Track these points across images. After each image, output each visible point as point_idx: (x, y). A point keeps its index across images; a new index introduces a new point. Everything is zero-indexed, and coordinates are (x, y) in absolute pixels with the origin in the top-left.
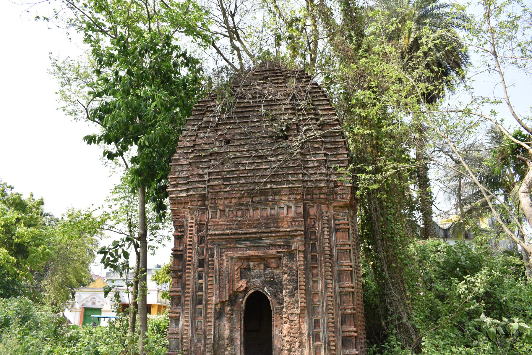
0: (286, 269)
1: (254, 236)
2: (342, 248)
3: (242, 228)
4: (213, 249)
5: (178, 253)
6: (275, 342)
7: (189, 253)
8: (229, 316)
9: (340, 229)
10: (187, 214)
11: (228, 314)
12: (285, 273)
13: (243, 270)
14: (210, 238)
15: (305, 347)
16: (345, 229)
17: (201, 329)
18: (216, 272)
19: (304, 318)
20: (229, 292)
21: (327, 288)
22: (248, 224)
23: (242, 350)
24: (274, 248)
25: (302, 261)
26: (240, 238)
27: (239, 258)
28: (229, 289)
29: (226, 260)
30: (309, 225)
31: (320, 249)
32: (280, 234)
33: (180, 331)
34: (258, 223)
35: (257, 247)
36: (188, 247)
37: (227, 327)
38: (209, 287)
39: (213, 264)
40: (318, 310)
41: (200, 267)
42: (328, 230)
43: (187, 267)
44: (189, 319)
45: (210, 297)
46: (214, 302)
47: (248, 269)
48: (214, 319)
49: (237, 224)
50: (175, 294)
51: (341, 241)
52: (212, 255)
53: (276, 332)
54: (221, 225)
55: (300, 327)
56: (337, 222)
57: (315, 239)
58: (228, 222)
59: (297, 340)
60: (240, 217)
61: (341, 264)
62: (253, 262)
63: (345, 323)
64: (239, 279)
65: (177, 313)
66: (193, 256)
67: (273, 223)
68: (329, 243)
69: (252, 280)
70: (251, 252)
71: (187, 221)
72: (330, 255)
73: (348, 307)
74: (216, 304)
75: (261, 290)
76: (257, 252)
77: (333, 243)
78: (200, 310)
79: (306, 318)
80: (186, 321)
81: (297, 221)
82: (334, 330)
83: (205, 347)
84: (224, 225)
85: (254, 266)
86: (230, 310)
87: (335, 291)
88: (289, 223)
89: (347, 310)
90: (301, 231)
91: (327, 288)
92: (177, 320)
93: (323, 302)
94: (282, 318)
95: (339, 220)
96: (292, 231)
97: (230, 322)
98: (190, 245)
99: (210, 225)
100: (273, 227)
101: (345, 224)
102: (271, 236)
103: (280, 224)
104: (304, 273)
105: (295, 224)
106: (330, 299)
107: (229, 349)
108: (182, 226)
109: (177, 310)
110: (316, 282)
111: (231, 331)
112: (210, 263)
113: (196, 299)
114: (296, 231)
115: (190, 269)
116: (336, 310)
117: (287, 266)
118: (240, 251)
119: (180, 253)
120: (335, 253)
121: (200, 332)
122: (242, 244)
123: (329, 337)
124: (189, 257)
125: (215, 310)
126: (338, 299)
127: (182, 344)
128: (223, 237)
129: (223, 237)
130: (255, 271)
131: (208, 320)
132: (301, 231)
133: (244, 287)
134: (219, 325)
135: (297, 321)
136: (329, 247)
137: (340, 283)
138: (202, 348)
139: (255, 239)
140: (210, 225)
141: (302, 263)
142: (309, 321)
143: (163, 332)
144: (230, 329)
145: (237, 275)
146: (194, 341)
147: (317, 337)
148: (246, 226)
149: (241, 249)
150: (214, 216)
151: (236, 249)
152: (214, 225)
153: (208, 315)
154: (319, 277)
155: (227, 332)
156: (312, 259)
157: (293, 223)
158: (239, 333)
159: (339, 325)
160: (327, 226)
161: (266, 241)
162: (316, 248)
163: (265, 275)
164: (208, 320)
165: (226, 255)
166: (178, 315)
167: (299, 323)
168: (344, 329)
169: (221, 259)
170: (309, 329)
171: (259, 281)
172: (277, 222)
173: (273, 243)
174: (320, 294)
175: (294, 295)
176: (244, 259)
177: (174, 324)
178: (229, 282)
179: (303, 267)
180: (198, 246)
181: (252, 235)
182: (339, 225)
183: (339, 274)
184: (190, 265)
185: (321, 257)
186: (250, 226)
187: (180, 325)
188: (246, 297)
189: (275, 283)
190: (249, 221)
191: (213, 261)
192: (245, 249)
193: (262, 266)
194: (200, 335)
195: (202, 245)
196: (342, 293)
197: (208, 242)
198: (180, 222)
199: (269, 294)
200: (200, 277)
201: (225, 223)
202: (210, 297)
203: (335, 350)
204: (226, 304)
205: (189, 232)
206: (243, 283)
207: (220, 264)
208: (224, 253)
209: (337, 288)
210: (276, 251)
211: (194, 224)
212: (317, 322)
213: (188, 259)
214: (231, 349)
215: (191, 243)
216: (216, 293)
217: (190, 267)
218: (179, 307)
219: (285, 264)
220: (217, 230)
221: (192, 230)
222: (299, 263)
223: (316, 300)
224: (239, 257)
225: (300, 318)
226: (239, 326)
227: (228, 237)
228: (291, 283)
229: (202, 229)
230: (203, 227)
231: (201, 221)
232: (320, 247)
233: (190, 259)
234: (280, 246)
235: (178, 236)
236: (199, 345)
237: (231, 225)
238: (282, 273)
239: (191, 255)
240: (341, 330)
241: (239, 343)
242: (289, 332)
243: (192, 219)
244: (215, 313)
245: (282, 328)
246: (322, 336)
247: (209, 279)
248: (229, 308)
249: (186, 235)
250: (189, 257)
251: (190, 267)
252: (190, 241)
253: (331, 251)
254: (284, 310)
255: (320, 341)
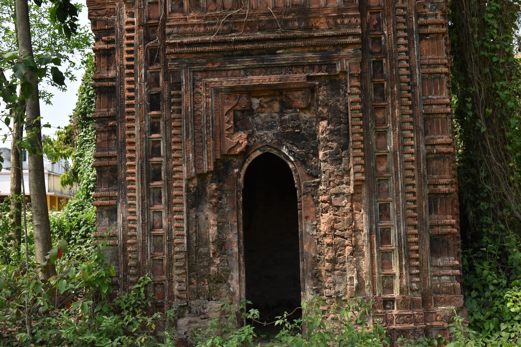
0: (325, 111)
1: (261, 45)
2: (432, 70)
3: (236, 31)
4: (179, 72)
5: (105, 84)
6: (305, 247)
7: (129, 82)
8: (214, 200)
9: (428, 34)
10: (120, 6)
11: (213, 196)
12: (323, 119)
13: (239, 114)
14: (172, 50)
15: (363, 255)
16: (438, 34)
17: (161, 227)
18: (187, 117)
19: (360, 201)
20: (215, 155)
21: (405, 146)
22: (248, 24)
23: (242, 263)
24: (300, 70)
25: (356, 94)
26: (232, 51)
27: (232, 91)
28: (215, 149)
29: (207, 93)
30: (368, 25)
31: (391, 72)
32: (314, 42)
33: (119, 231)
34: (269, 21)
35: (267, 68)
36: (127, 71)
37: (212, 222)
38: (173, 147)
39: (180, 103)
40: (387, 186)
41: (152, 110)
42: (406, 34)
43: (127, 110)
44: (137, 210)
45: (176, 166)
46: (185, 175)
47: (249, 111)
48: (187, 207)
49: (224, 24)
50: (105, 162)
51: (429, 58)
52: (178, 86)
53: (306, 228)
54: (193, 25)
55: (353, 219)
56: (422, 20)
57: (380, 52)
58: (207, 18)
59: (347, 242)
60: (230, 9)
61: (428, 101)
62: (258, 98)
63: (436, 210)
64: (232, 131)
65: (111, 198)
66: (138, 87)
67: (298, 20)
68: (407, 61)
69: (258, 133)
70: (255, 78)
71: (120, 19)
72: (409, 84)
73: (441, 181)
74: (189, 180)
75: (275, 152)
76: (267, 77)
77: (415, 61)
78: (156, 192)
79: (364, 201)
80: (131, 213)
81: (347, 16)
82: (416, 222)
83: (170, 259)
84: (199, 25)
85: (261, 106)
86: (216, 190)
87: (418, 151)
88: (331, 21)
89: (440, 187)
90: (354, 35)
91: (405, 146)
92: (112, 212)
93: (396, 172)
94: (317, 203)
95: (426, 16)
96: (338, 36)
97: (217, 212)
98: (129, 67)
99: (170, 26)
100: (299, 28)
101: (437, 25)
102: (295, 47)
103: (313, 22)
104: (361, 118)
105: (342, 23)
106: (410, 166)
107: (217, 261)
108: (112, 31)
109: (112, 193)
110: (383, 134)
111: (220, 228)
112: (173, 100)
113: (148, 171)
114: (346, 35)
115: (132, 113)
116: (420, 186)
117: (326, 105)
118: (232, 76)
119: (110, 83)
120: (418, 80)
121: (160, 231)
122: (236, 63)
123: (407, 235)
124: (130, 90)
125: (188, 190)
126: (423, 166)
127: (125, 256)
128: (199, 49)
129: (199, 49)
130: (263, 115)
131: (174, 208)
132: (354, 35)
133: (243, 145)
134: (197, 217)
135: (348, 207)
136: (407, 68)
137: (427, 137)
138: (165, 262)
139: (262, 52)
140: (170, 26)
141: (357, 98)
142: (371, 206)
143: (69, 235)
144: (217, 226)
145: (228, 122)
146: (150, 250)
147: (384, 237)
148: (243, 26)
149: (234, 73)
150: (177, 7)
151: (224, 73)
152: (179, 26)
153: (174, 201)
154: (390, 125)
155: (213, 231)
156: (375, 91)
157: (339, 21)
158: (236, 231)
159: (425, 213)
160: (402, 26)
161: (286, 56)
162: (382, 71)
163: (282, 122)
164: (174, 208)
165: (206, 85)
166: (113, 202)
167: (352, 210)
168: (435, 222)
169: (195, 93)
170: (371, 221)
171: (270, 134)
172: (307, 19)
173: (298, 59)
174: (390, 157)
175: (340, 159)
176: (241, 93)
177: (107, 219)
178: (214, 137)
179: (358, 106)
180: (146, 69)
181: (256, 45)
182: (426, 26)
183: (425, 120)
184: (132, 105)
185: (392, 88)
186: (251, 26)
187: (120, 221)
188: (246, 165)
189: (303, 138)
190: (250, 16)
191: (179, 96)
192: (242, 72)
193: (276, 106)
194: (159, 238)
195: (154, 67)
196: (430, 156)
197: (166, 61)
198: (106, 22)
199: (292, 159)
200: (154, 129)
201: (202, 21)
202: (176, 166)
203: (417, 259)
204: (209, 179)
205: (126, 42)
206: (241, 138)
207: (195, 103)
208: (200, 80)
209: (422, 146)
210: (304, 75)
211: (136, 26)
212: (384, 209)
213: (127, 94)
214: (221, 261)
215: (132, 63)
216: (188, 158)
217: (133, 109)
218: (114, 187)
219: (323, 101)
220: (184, 35)
221: (132, 38)
222: (350, 99)
223: (382, 168)
224: (231, 88)
225: (352, 201)
226: (234, 219)
227: (207, 48)
228: (335, 137)
229: (152, 35)
230: (154, 31)
231: (149, 19)
232: (391, 68)
233: (132, 94)
234: (312, 66)
235: (104, 50)
236: (159, 255)
237: (212, 25)
238: (317, 118)
239: (132, 86)
240: (428, 224)
241: (236, 250)
242: (333, 229)
243: (132, 15)
244: (187, 196)
245: (319, 221)
246: (393, 234)
247: (173, 132)
248: (214, 186)
249: (121, 48)
250: (130, 90)
251: (133, 109)
252: (128, 59)
253: (411, 76)
254: (321, 187)
255: (389, 242)
